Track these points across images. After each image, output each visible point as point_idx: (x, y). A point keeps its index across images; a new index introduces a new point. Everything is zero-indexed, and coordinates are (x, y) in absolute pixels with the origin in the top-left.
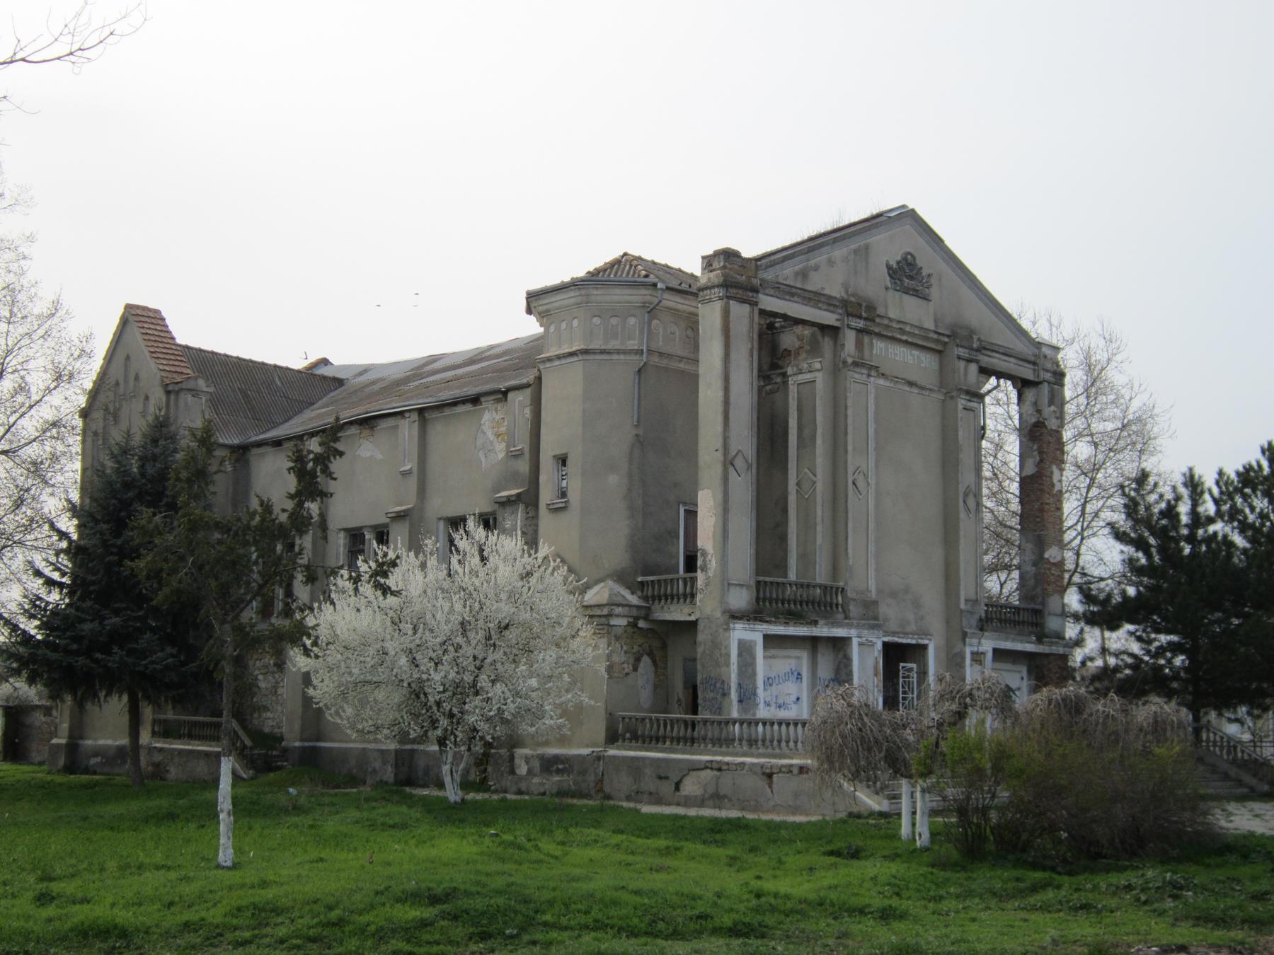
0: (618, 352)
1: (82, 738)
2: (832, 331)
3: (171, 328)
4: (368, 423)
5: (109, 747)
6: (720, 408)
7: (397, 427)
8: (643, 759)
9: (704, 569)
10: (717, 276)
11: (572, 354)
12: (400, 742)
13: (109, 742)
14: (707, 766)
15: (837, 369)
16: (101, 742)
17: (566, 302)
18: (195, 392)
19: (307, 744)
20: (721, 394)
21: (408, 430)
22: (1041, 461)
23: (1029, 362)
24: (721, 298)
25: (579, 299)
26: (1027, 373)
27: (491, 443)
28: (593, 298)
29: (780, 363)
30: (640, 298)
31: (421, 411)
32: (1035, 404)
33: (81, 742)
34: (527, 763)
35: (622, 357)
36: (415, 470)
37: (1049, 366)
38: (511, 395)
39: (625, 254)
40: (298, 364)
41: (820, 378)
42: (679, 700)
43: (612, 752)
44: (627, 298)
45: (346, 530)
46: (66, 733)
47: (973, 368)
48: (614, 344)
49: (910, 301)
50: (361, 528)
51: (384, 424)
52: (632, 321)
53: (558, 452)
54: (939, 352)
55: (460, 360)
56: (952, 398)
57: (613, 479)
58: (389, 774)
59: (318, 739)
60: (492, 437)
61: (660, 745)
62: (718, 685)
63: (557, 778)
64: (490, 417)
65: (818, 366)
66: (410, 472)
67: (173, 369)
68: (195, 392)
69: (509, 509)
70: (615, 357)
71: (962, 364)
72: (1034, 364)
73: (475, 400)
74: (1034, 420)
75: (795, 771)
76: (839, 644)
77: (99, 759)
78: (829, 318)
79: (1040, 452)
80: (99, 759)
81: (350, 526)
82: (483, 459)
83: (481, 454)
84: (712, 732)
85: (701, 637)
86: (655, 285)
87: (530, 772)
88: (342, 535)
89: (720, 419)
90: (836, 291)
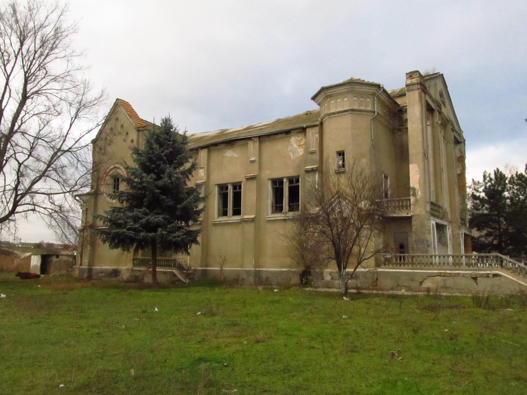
1: (93, 266)
3: (134, 109)
7: (248, 144)
8: (401, 272)
9: (414, 195)
10: (416, 80)
11: (346, 111)
12: (255, 267)
13: (108, 267)
14: (440, 275)
16: (104, 267)
19: (203, 268)
21: (253, 147)
24: (418, 89)
25: (349, 90)
28: (355, 89)
29: (404, 124)
30: (372, 91)
33: (93, 267)
34: (330, 275)
35: (366, 113)
36: (257, 160)
38: (308, 130)
43: (379, 270)
46: (87, 264)
48: (362, 108)
50: (226, 184)
51: (238, 143)
53: (339, 149)
58: (252, 279)
59: (207, 266)
60: (295, 146)
61: (406, 266)
62: (425, 242)
64: (294, 141)
69: (311, 175)
70: (363, 113)
73: (288, 132)
74: (459, 155)
75: (491, 276)
77: (103, 274)
80: (103, 274)
81: (219, 183)
82: (292, 155)
83: (291, 154)
84: (424, 260)
85: (414, 223)
87: (332, 278)
88: (216, 187)
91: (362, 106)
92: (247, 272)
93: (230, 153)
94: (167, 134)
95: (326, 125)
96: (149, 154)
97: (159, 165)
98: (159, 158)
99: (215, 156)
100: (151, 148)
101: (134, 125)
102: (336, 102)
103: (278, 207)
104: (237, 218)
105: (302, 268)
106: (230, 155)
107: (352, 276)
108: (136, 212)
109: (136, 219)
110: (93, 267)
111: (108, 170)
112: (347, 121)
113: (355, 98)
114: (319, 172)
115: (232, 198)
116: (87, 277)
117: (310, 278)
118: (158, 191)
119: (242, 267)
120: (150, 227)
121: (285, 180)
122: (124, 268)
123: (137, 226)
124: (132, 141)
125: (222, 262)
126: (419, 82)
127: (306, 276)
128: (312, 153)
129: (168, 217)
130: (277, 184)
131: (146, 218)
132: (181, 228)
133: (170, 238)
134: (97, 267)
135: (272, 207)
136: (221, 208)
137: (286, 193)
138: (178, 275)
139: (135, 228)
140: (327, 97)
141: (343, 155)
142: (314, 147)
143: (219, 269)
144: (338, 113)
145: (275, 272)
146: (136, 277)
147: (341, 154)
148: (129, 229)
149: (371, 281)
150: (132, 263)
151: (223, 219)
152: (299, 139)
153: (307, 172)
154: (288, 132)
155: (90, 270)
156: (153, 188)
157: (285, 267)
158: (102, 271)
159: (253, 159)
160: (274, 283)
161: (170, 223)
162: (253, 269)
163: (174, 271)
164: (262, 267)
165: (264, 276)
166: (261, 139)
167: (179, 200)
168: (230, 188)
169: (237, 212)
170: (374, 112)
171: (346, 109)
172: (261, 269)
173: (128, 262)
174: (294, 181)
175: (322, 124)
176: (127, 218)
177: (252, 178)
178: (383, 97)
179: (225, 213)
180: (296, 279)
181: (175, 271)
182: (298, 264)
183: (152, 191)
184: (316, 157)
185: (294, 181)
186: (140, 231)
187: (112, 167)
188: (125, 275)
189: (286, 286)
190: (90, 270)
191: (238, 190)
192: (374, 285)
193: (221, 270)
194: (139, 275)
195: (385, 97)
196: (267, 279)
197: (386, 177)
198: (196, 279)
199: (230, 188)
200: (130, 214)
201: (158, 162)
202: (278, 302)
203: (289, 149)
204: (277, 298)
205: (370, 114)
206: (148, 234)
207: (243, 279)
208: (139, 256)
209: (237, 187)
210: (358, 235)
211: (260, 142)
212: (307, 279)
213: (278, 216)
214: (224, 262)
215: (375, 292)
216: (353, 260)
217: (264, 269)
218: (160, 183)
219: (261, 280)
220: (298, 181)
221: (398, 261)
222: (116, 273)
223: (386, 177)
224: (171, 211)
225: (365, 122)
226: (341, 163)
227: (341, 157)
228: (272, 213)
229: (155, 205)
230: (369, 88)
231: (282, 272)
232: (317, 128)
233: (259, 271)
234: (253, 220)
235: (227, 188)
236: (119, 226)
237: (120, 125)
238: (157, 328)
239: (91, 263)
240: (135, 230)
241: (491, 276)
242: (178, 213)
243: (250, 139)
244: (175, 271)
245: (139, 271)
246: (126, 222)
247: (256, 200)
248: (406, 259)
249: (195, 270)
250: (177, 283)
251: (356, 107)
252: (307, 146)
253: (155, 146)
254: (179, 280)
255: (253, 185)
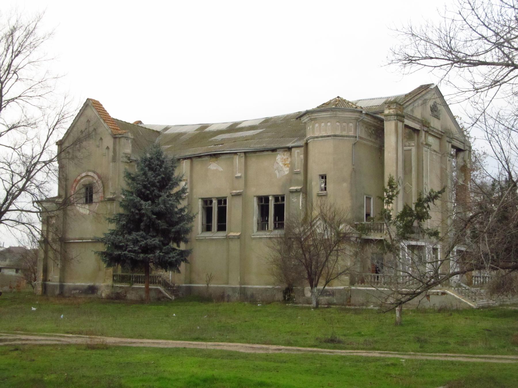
0: (347, 136)
1: (64, 282)
2: (416, 131)
3: (106, 109)
4: (215, 156)
5: (83, 286)
6: (395, 161)
7: (233, 158)
11: (328, 136)
13: (83, 284)
15: (419, 147)
16: (78, 284)
17: (325, 116)
18: (127, 138)
20: (395, 156)
21: (238, 161)
22: (465, 179)
23: (462, 142)
24: (395, 120)
26: (461, 147)
27: (282, 167)
28: (338, 115)
31: (245, 153)
32: (463, 158)
33: (65, 284)
35: (348, 138)
36: (243, 176)
37: (468, 144)
38: (293, 150)
39: (338, 97)
40: (132, 122)
41: (414, 149)
42: (369, 268)
44: (350, 116)
45: (202, 199)
47: (450, 145)
48: (344, 133)
49: (436, 120)
50: (211, 198)
51: (223, 157)
52: (351, 124)
53: (322, 173)
54: (439, 138)
55: (224, 127)
56: (444, 156)
57: (345, 185)
59: (190, 283)
60: (281, 164)
63: (327, 298)
64: (280, 158)
65: (413, 144)
66: (240, 177)
67: (112, 127)
68: (127, 138)
69: (295, 194)
70: (345, 138)
71: (448, 143)
72: (464, 143)
73: (274, 150)
74: (462, 164)
75: (440, 294)
76: (420, 248)
78: (417, 126)
79: (465, 176)
80: (78, 291)
81: (203, 197)
82: (278, 174)
83: (276, 172)
86: (361, 112)
88: (200, 200)
89: (395, 165)
90: (419, 117)
91: (344, 130)
92: (234, 289)
93: (214, 166)
94: (158, 159)
95: (310, 146)
96: (145, 181)
97: (153, 191)
98: (153, 185)
99: (198, 165)
100: (145, 174)
101: (110, 131)
102: (320, 126)
103: (263, 225)
104: (221, 234)
105: (285, 286)
106: (215, 168)
107: (323, 292)
108: (134, 235)
109: (136, 242)
110: (65, 284)
111: (79, 178)
112: (329, 145)
113: (338, 124)
114: (303, 193)
115: (217, 213)
116: (59, 294)
117: (292, 294)
118: (155, 216)
119: (227, 284)
120: (146, 250)
121: (270, 198)
122: (102, 284)
123: (137, 248)
124: (108, 148)
125: (208, 279)
126: (395, 113)
127: (288, 294)
128: (297, 173)
129: (162, 239)
130: (263, 201)
131: (145, 241)
132: (174, 249)
133: (167, 258)
134: (69, 284)
135: (258, 224)
136: (205, 222)
137: (272, 210)
138: (164, 292)
139: (135, 250)
140: (311, 120)
141: (326, 178)
142: (299, 168)
143: (205, 285)
144: (322, 137)
145: (261, 289)
146: (118, 293)
147: (324, 177)
148: (129, 251)
149: (345, 297)
150: (112, 279)
151: (208, 234)
152: (285, 157)
153: (292, 192)
154: (274, 150)
155: (62, 287)
156: (142, 205)
157: (269, 285)
158: (76, 288)
159: (239, 175)
160: (259, 300)
161: (164, 245)
162: (238, 286)
163: (159, 287)
164: (248, 284)
165: (249, 293)
166: (247, 155)
167: (173, 224)
168: (215, 202)
169: (222, 227)
170: (356, 137)
171: (328, 134)
172: (246, 286)
173: (108, 279)
174: (279, 200)
175: (307, 144)
176: (127, 241)
177: (238, 195)
178: (367, 119)
179: (208, 228)
180: (280, 296)
181: (161, 288)
182: (281, 281)
183: (149, 218)
184: (301, 178)
185: (279, 200)
186: (139, 253)
187: (84, 174)
188: (104, 293)
189: (268, 302)
190: (62, 287)
191: (222, 205)
192: (348, 300)
193: (208, 287)
194: (121, 292)
195: (369, 119)
196: (252, 296)
197: (368, 198)
198: (180, 295)
199: (215, 202)
200: (130, 238)
201: (152, 189)
202: (260, 311)
203: (275, 166)
204: (259, 309)
205: (352, 139)
206: (147, 255)
207: (228, 296)
208: (119, 272)
209: (222, 202)
210: (327, 260)
211: (246, 157)
212: (290, 295)
213: (264, 234)
214: (210, 279)
215: (347, 307)
216: (322, 281)
217: (249, 286)
218: (157, 209)
219: (247, 297)
220: (283, 199)
221: (376, 280)
222: (92, 289)
223: (368, 198)
224: (165, 233)
225: (346, 146)
226: (323, 185)
227: (324, 180)
228: (258, 230)
229: (151, 228)
230: (352, 114)
231: (267, 290)
232: (302, 149)
233: (245, 288)
234: (239, 237)
235: (211, 202)
236: (120, 248)
237: (99, 138)
238: (151, 340)
239: (62, 280)
240: (135, 252)
241: (440, 294)
242: (172, 235)
243: (236, 153)
244: (161, 288)
245: (121, 287)
246: (127, 245)
247: (242, 216)
248: (379, 279)
249: (179, 287)
250: (162, 299)
251: (338, 133)
252: (292, 166)
253: (150, 173)
254: (164, 297)
255: (238, 201)
